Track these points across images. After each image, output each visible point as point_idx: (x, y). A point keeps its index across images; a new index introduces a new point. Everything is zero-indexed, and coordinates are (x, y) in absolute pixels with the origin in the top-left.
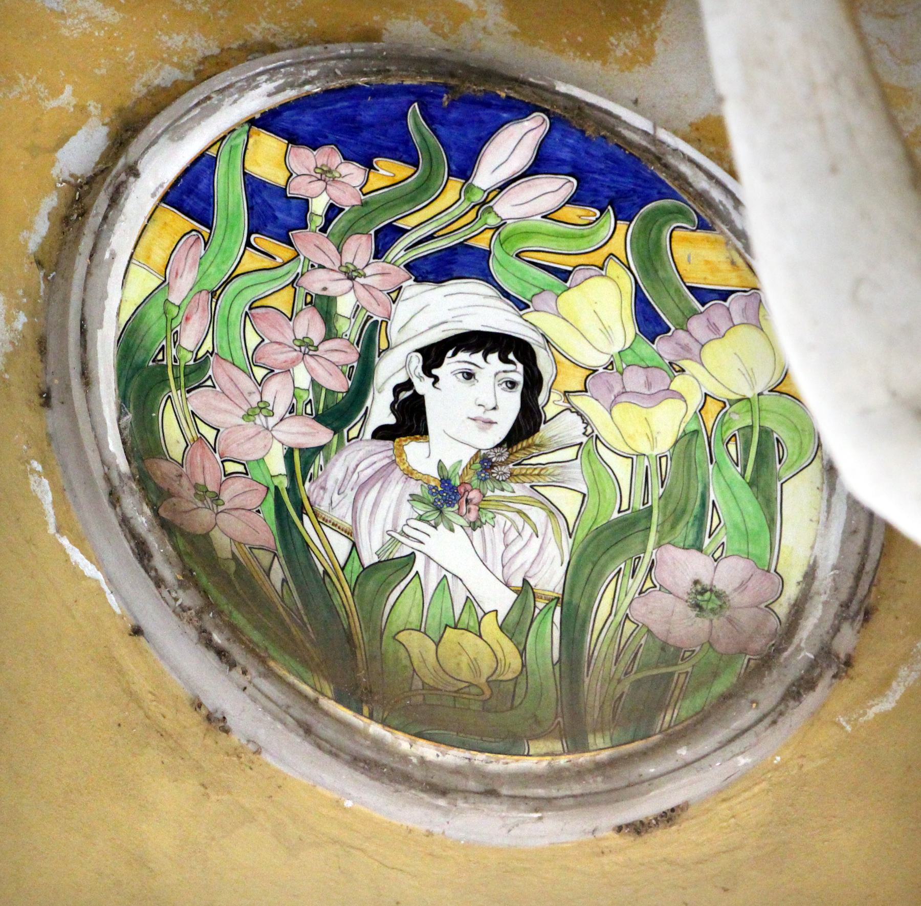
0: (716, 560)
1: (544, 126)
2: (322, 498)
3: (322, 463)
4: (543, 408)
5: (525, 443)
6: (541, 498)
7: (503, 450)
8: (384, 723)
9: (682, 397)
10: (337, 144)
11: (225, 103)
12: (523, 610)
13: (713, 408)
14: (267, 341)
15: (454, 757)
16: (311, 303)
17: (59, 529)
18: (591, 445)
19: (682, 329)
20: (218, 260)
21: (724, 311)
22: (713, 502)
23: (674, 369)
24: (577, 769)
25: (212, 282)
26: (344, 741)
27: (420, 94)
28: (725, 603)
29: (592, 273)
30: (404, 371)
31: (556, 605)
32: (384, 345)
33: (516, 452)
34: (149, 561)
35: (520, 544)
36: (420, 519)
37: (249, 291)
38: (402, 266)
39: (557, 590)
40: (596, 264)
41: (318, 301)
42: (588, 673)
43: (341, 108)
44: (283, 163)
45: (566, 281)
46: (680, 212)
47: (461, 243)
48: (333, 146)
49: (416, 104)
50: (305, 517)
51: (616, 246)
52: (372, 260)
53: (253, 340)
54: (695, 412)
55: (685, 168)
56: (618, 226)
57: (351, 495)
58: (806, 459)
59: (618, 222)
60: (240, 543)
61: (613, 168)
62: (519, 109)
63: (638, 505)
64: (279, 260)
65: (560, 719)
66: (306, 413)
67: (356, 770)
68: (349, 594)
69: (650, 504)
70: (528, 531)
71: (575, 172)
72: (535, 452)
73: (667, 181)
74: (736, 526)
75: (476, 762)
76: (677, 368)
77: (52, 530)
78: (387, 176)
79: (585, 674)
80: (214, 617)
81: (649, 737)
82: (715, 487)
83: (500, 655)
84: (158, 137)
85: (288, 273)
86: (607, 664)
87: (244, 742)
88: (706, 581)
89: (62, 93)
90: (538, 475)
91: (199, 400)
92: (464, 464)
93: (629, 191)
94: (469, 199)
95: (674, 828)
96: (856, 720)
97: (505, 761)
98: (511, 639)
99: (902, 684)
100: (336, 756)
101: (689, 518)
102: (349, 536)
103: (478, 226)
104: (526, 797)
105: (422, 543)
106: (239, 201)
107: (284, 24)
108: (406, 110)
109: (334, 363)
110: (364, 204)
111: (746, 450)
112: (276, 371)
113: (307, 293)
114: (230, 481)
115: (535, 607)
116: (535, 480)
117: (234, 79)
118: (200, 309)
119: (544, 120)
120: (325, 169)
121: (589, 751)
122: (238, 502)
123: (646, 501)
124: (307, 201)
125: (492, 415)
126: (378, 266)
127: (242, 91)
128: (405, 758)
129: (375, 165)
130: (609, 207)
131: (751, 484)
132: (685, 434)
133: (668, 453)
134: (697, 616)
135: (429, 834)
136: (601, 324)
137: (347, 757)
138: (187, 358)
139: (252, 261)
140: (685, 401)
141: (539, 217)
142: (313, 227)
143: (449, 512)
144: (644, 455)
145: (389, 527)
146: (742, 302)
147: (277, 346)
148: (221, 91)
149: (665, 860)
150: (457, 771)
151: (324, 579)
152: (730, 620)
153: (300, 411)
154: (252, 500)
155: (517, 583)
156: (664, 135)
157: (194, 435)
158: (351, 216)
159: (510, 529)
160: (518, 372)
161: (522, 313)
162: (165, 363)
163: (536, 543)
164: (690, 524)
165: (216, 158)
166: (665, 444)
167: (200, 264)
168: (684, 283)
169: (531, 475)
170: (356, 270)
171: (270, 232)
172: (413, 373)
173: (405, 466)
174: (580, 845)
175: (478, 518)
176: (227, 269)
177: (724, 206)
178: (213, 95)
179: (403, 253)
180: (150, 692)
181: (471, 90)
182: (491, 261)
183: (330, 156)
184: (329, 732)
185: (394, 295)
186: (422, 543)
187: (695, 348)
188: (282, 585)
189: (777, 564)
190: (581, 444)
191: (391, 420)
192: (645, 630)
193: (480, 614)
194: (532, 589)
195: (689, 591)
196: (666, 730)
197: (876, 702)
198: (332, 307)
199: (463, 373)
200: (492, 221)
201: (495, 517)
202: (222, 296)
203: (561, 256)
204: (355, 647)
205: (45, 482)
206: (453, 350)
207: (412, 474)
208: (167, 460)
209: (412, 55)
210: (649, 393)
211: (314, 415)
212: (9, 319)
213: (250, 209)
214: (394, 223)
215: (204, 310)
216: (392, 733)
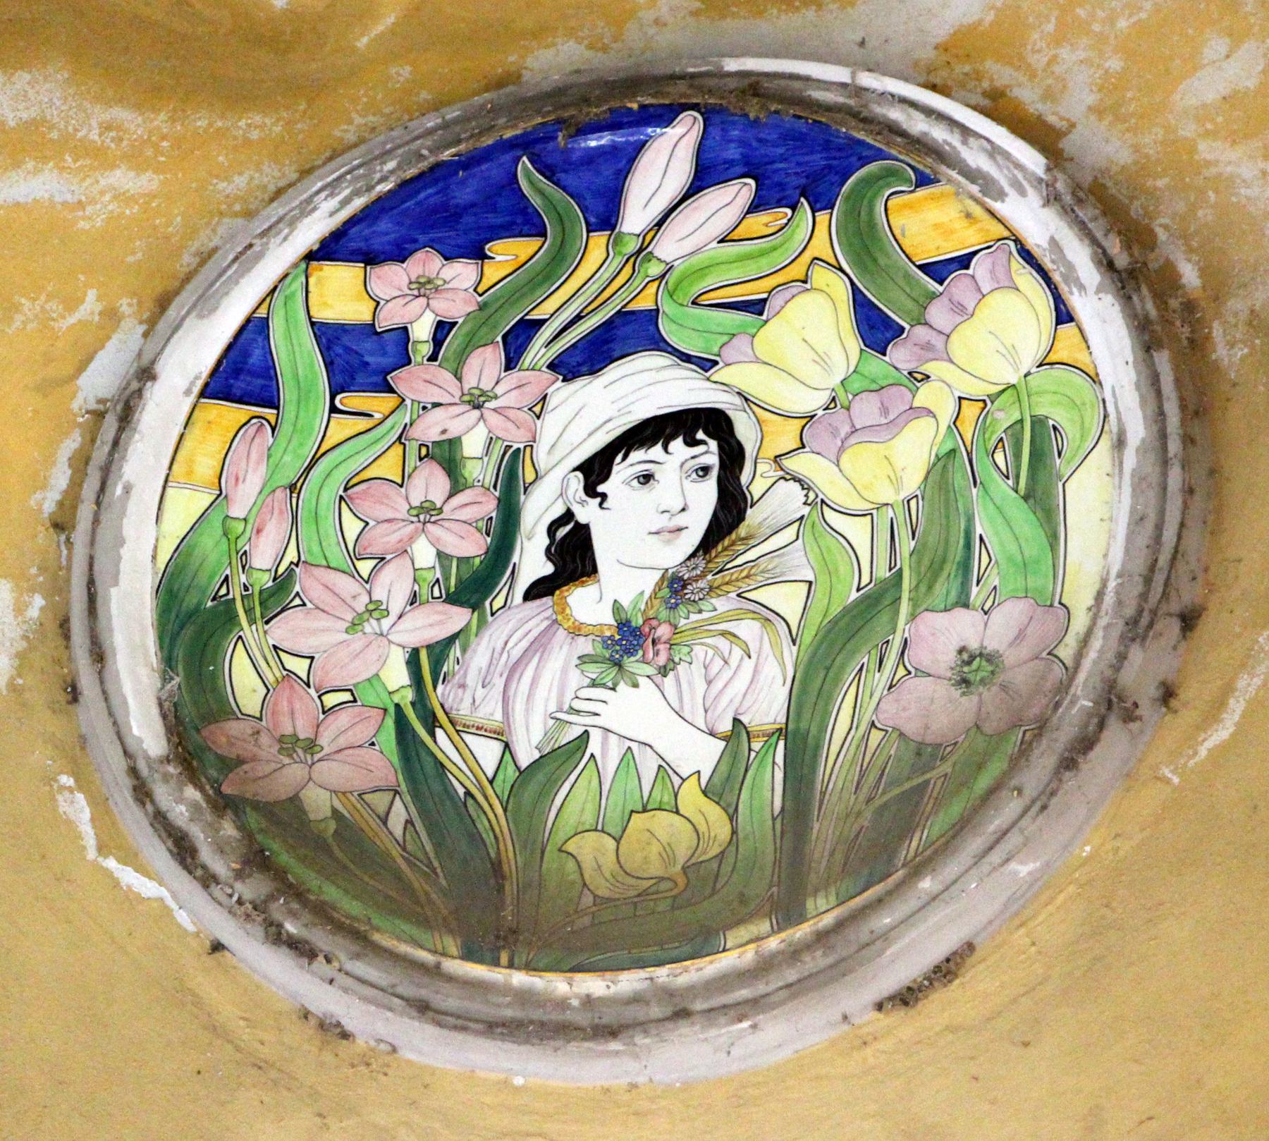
0: (986, 613)
1: (696, 126)
2: (462, 700)
3: (458, 654)
4: (747, 487)
5: (726, 542)
6: (752, 606)
7: (700, 561)
8: (529, 967)
9: (930, 413)
10: (430, 244)
11: (271, 246)
12: (735, 757)
13: (970, 411)
14: (372, 523)
15: (629, 982)
16: (427, 456)
17: (102, 849)
18: (816, 516)
19: (920, 324)
20: (295, 442)
21: (967, 281)
22: (981, 537)
23: (915, 379)
24: (792, 949)
25: (290, 475)
26: (476, 1007)
27: (524, 144)
28: (997, 666)
29: (794, 291)
30: (560, 500)
31: (778, 739)
32: (530, 476)
33: (716, 557)
34: (193, 859)
35: (727, 674)
36: (594, 684)
37: (341, 468)
38: (544, 369)
39: (778, 720)
40: (797, 278)
41: (436, 450)
42: (818, 815)
43: (427, 198)
44: (365, 293)
45: (761, 314)
46: (891, 174)
47: (619, 312)
48: (427, 249)
49: (525, 158)
50: (439, 732)
51: (820, 246)
52: (503, 374)
53: (352, 527)
54: (949, 426)
55: (896, 114)
56: (818, 219)
57: (499, 683)
58: (1090, 439)
59: (817, 214)
60: (344, 793)
61: (795, 148)
62: (661, 116)
63: (883, 572)
64: (378, 416)
65: (775, 889)
66: (433, 598)
67: (494, 1039)
68: (499, 811)
69: (898, 567)
70: (737, 653)
71: (751, 169)
72: (742, 548)
73: (869, 140)
74: (1010, 559)
75: (661, 980)
76: (919, 377)
77: (92, 854)
78: (507, 261)
79: (815, 819)
80: (286, 903)
81: (890, 876)
82: (982, 516)
83: (702, 828)
84: (183, 319)
85: (392, 428)
86: (845, 795)
87: (372, 1043)
88: (974, 645)
89: (83, 302)
90: (747, 577)
91: (283, 630)
92: (647, 595)
93: (823, 169)
94: (620, 253)
95: (957, 982)
96: (1186, 764)
97: (696, 967)
98: (717, 803)
99: (1241, 699)
100: (464, 1029)
101: (951, 568)
102: (500, 737)
103: (638, 283)
104: (725, 1006)
105: (597, 715)
106: (312, 362)
107: (387, 111)
108: (513, 170)
109: (465, 522)
110: (482, 307)
111: (1018, 455)
112: (389, 557)
113: (421, 445)
114: (331, 718)
115: (750, 750)
116: (753, 583)
117: (281, 211)
118: (276, 512)
119: (695, 118)
120: (422, 280)
121: (808, 920)
122: (342, 742)
123: (893, 565)
124: (405, 329)
125: (681, 520)
126: (515, 377)
127: (293, 223)
128: (562, 1004)
129: (489, 253)
130: (802, 200)
131: (1026, 498)
132: (938, 459)
133: (918, 493)
134: (964, 694)
135: (633, 1086)
136: (813, 352)
137: (480, 1027)
138: (266, 581)
139: (342, 427)
140: (934, 416)
141: (714, 244)
142: (419, 359)
143: (631, 664)
144: (887, 504)
145: (552, 707)
146: (989, 261)
147: (386, 525)
148: (264, 234)
149: (947, 1028)
150: (636, 999)
151: (465, 804)
152: (1004, 688)
153: (424, 598)
154: (362, 733)
155: (726, 726)
156: (867, 80)
157: (278, 675)
158: (465, 330)
159: (712, 660)
160: (711, 453)
161: (708, 374)
162: (231, 596)
163: (749, 665)
164: (952, 576)
165: (267, 318)
166: (913, 481)
167: (269, 457)
168: (913, 263)
169: (737, 580)
170: (483, 393)
171: (362, 384)
172: (572, 500)
173: (570, 623)
174: (833, 1043)
175: (670, 660)
176: (308, 451)
177: (949, 144)
178: (254, 241)
179: (544, 350)
180: (242, 1018)
181: (592, 115)
182: (660, 320)
183: (426, 263)
184: (450, 1001)
185: (537, 409)
186: (597, 715)
187: (938, 341)
188: (405, 829)
189: (1062, 592)
190: (802, 517)
191: (549, 569)
192: (895, 735)
193: (677, 781)
194: (745, 728)
195: (953, 665)
196: (911, 861)
197: (1209, 733)
198: (455, 452)
199: (638, 477)
200: (655, 269)
201: (692, 650)
202: (304, 487)
203: (752, 283)
204: (503, 877)
205: (80, 797)
206: (623, 452)
207: (579, 629)
208: (238, 718)
209: (529, 95)
210: (886, 421)
211: (444, 596)
212: (19, 609)
213: (329, 365)
214: (527, 317)
215: (281, 512)
216: (540, 977)
